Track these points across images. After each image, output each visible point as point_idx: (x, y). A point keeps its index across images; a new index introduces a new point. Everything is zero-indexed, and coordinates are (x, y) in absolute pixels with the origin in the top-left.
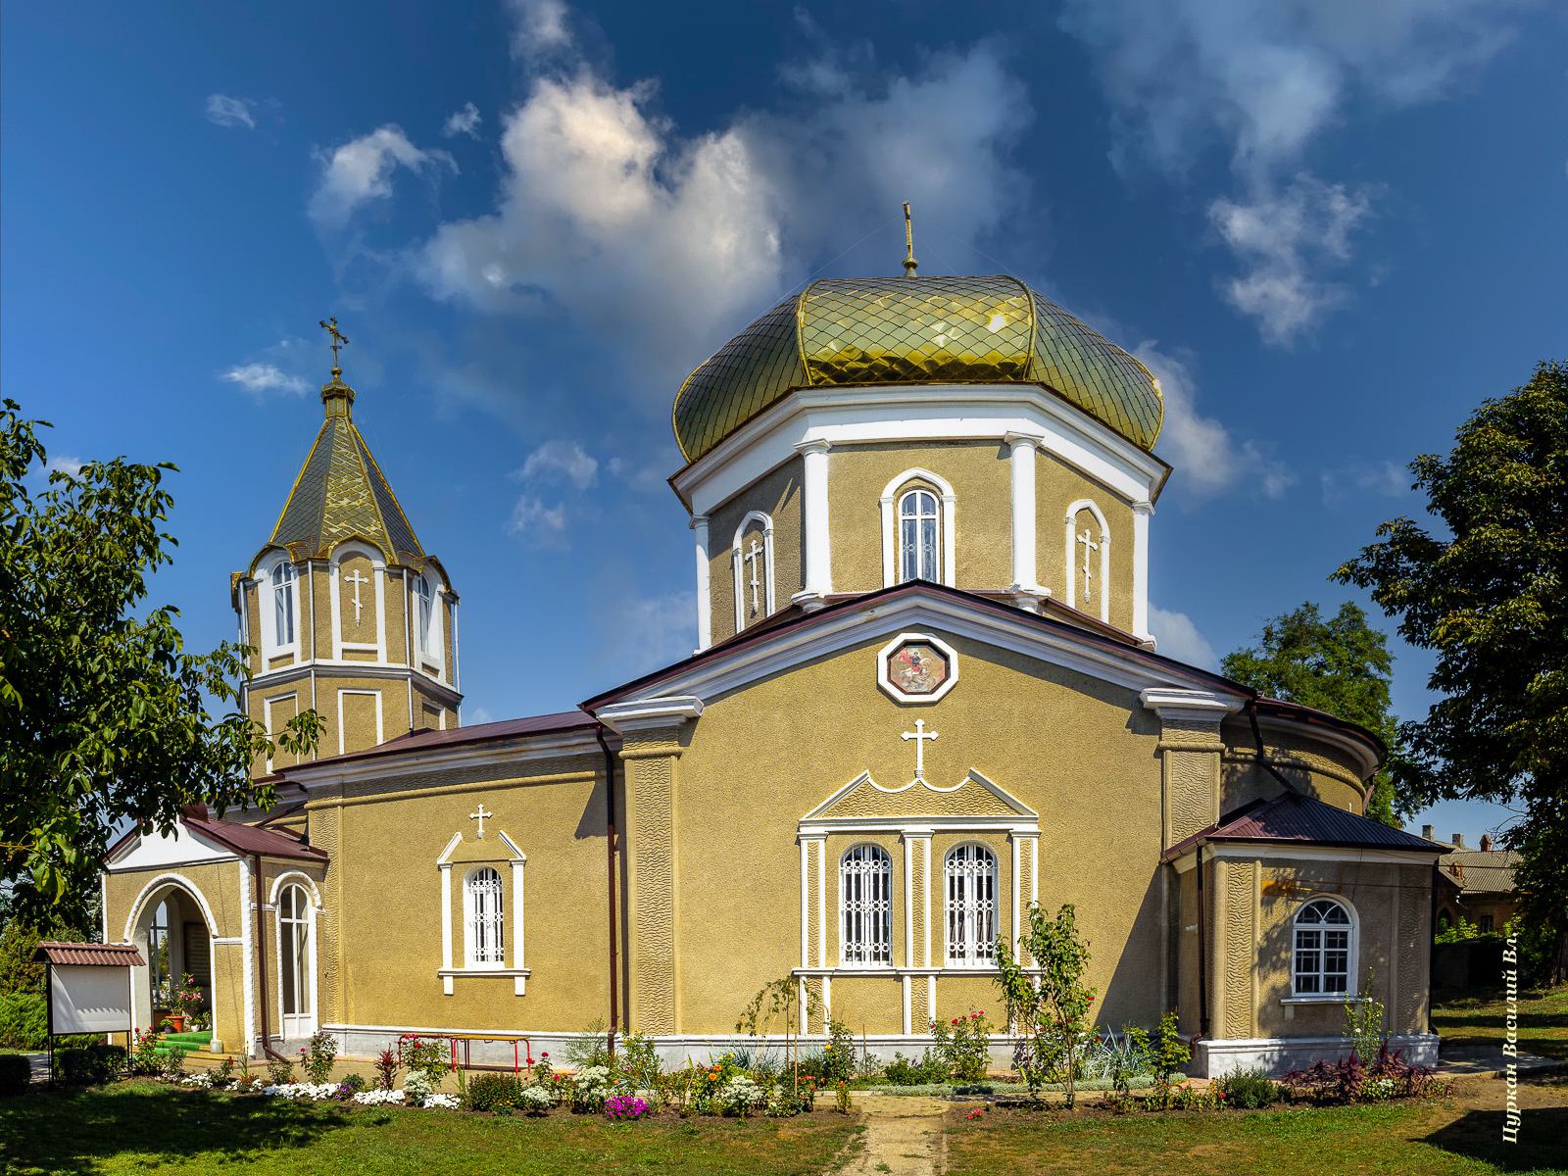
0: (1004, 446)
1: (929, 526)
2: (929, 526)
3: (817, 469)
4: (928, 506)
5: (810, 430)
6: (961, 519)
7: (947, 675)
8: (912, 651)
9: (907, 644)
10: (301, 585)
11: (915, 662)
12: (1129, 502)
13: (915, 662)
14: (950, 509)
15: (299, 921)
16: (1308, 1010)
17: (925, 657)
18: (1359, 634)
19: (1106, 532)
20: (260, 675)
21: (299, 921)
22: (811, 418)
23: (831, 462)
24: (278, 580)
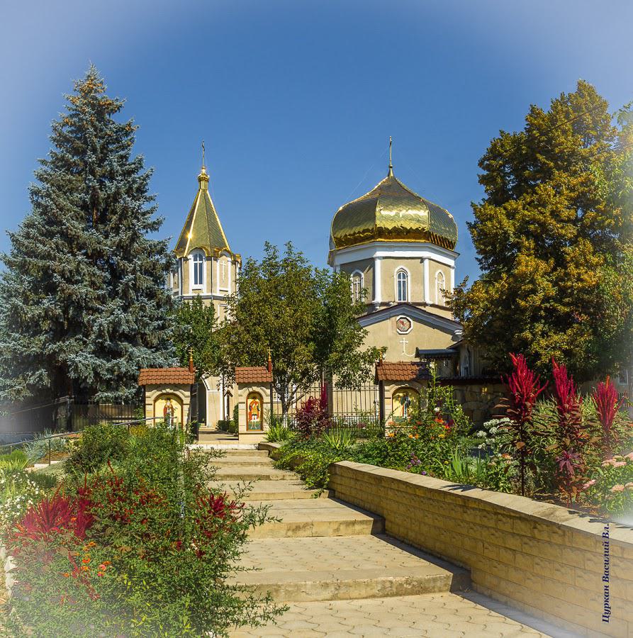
0: (422, 260)
1: (404, 282)
2: (404, 282)
3: (378, 263)
4: (404, 277)
5: (377, 252)
6: (412, 281)
7: (410, 327)
8: (402, 320)
9: (401, 318)
10: (208, 264)
11: (403, 323)
12: (449, 266)
13: (403, 323)
14: (409, 278)
15: (196, 262)
16: (437, 497)
17: (405, 321)
18: (572, 117)
19: (444, 279)
20: (187, 295)
21: (196, 262)
22: (378, 249)
23: (381, 263)
24: (195, 260)
